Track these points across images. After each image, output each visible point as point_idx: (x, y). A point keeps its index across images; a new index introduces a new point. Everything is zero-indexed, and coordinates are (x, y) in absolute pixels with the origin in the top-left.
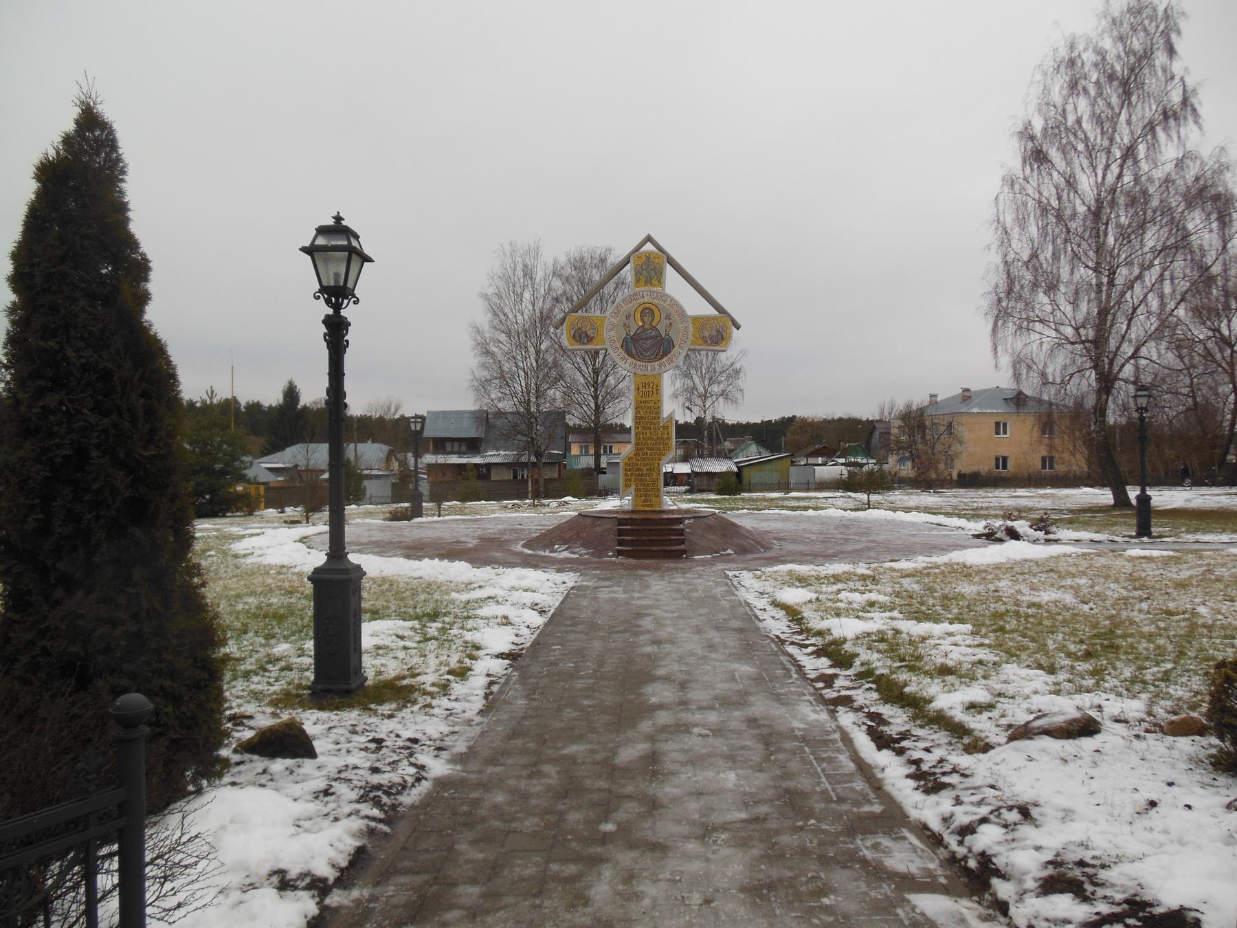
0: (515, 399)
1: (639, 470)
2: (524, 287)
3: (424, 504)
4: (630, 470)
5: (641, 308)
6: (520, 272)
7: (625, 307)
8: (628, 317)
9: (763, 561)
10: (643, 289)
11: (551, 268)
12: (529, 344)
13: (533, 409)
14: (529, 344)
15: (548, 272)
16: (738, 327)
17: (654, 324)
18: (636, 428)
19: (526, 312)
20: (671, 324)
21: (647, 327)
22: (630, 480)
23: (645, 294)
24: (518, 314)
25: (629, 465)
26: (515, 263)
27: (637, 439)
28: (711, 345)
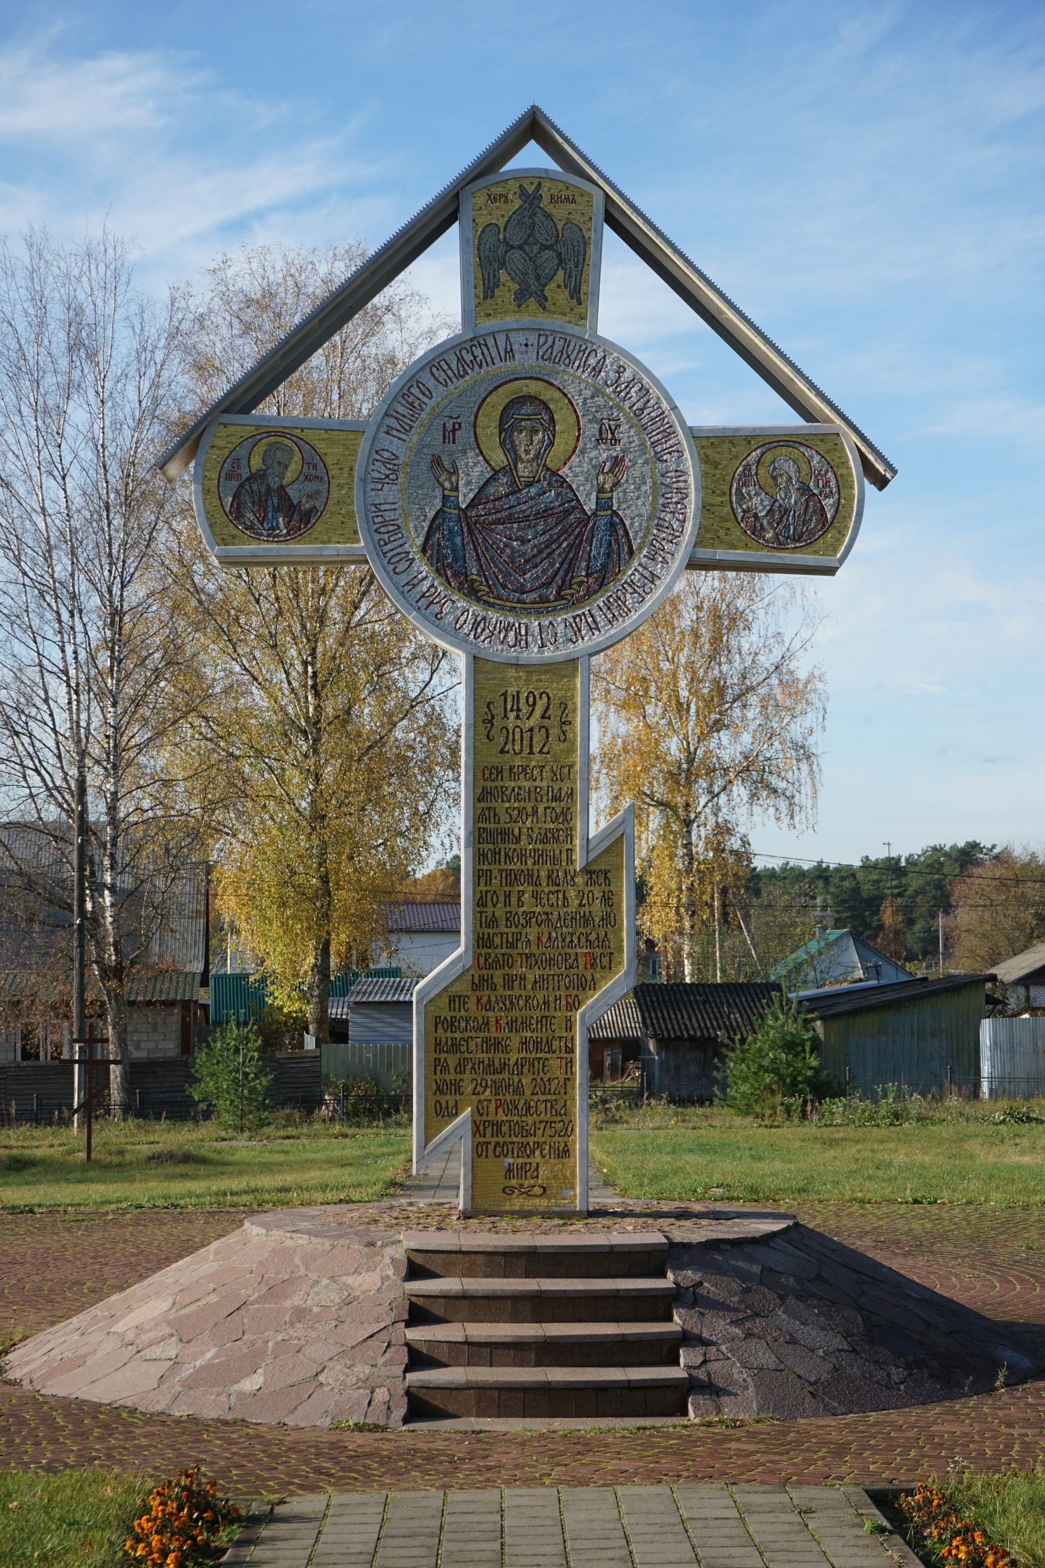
0: (34, 780)
1: (496, 1045)
2: (69, 390)
3: (688, 980)
4: (454, 1047)
5: (500, 399)
6: (58, 339)
7: (439, 392)
8: (449, 434)
9: (557, 1221)
10: (510, 320)
11: (163, 321)
12: (82, 585)
13: (97, 811)
14: (82, 585)
15: (152, 332)
16: (882, 483)
17: (552, 462)
18: (479, 876)
19: (76, 479)
20: (617, 462)
21: (523, 470)
22: (456, 1087)
23: (518, 339)
24: (50, 483)
25: (451, 1025)
26: (40, 301)
27: (483, 920)
28: (779, 544)
